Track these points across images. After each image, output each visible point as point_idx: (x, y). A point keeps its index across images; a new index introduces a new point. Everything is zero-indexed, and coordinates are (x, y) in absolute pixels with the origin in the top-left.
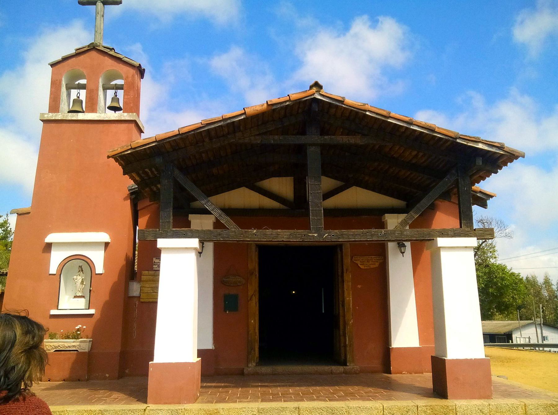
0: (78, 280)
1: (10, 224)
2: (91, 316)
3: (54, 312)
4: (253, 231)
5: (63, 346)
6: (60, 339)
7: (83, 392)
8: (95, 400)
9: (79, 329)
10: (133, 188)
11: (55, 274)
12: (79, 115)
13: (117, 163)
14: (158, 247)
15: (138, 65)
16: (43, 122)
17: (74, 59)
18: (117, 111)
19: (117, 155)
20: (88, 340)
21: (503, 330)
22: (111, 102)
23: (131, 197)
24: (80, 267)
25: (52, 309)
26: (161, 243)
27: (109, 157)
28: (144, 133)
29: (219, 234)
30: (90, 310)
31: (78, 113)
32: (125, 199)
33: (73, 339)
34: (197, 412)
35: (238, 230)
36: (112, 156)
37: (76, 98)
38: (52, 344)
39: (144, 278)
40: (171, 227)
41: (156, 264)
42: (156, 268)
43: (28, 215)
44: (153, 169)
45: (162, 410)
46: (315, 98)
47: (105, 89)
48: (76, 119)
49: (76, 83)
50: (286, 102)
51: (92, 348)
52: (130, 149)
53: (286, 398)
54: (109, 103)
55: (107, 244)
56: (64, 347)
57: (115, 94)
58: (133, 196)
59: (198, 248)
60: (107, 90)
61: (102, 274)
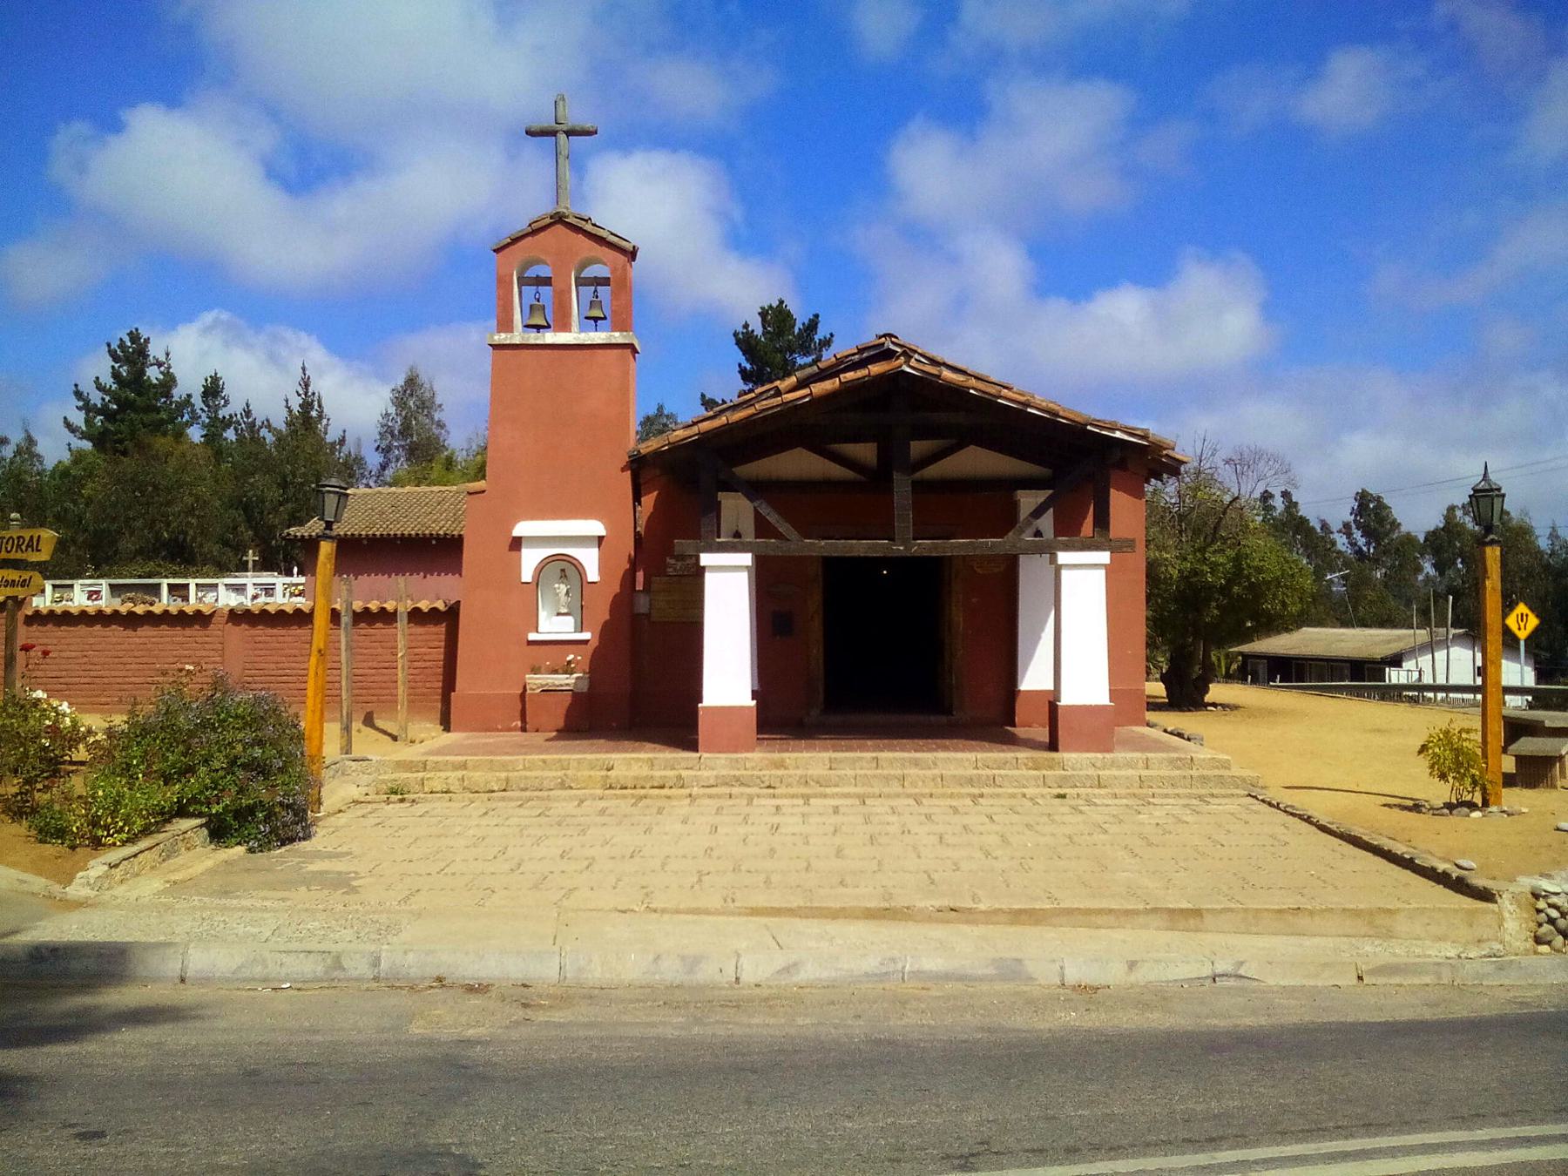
2: (585, 642)
3: (532, 636)
21: (1379, 652)
24: (563, 570)
25: (532, 632)
26: (706, 559)
32: (623, 470)
38: (537, 682)
46: (903, 371)
48: (542, 342)
50: (864, 377)
53: (862, 749)
55: (601, 538)
56: (555, 685)
58: (635, 466)
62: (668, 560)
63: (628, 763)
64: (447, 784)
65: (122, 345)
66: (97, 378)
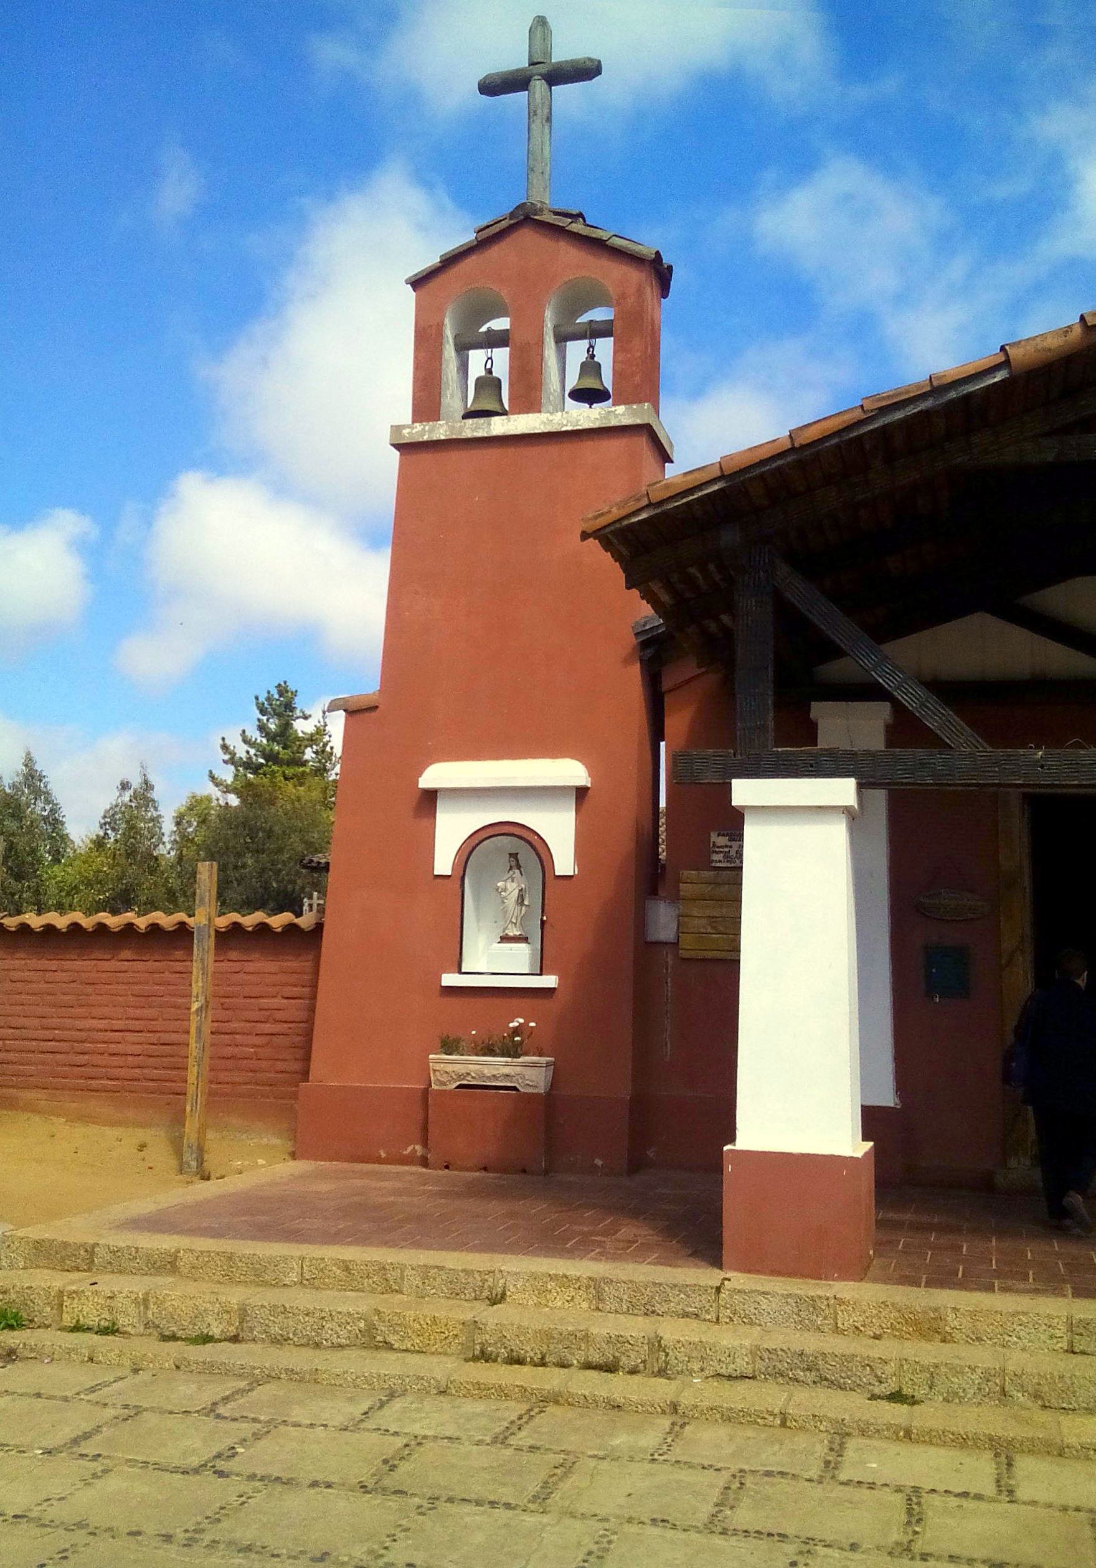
0: (508, 892)
1: (330, 736)
3: (450, 979)
4: (1036, 754)
5: (478, 1075)
6: (469, 1055)
7: (538, 1209)
8: (574, 1241)
9: (517, 1027)
10: (647, 628)
11: (450, 876)
12: (492, 423)
13: (609, 553)
14: (733, 804)
15: (653, 256)
16: (399, 451)
17: (472, 261)
18: (596, 402)
19: (607, 530)
20: (544, 1060)
22: (578, 377)
23: (642, 653)
27: (585, 536)
28: (672, 462)
29: (920, 764)
30: (543, 977)
31: (489, 418)
32: (627, 661)
33: (503, 1055)
34: (874, 1312)
35: (981, 749)
36: (594, 532)
37: (483, 373)
38: (449, 1068)
39: (685, 889)
40: (770, 743)
41: (717, 850)
42: (720, 861)
43: (373, 714)
44: (711, 567)
45: (767, 1294)
47: (562, 339)
49: (481, 330)
51: (554, 1084)
52: (647, 506)
54: (572, 382)
55: (581, 793)
56: (482, 1076)
57: (591, 353)
58: (649, 652)
59: (856, 806)
60: (566, 341)
61: (572, 876)
62: (714, 837)
63: (540, 1286)
64: (111, 1309)
65: (269, 699)
66: (244, 731)
